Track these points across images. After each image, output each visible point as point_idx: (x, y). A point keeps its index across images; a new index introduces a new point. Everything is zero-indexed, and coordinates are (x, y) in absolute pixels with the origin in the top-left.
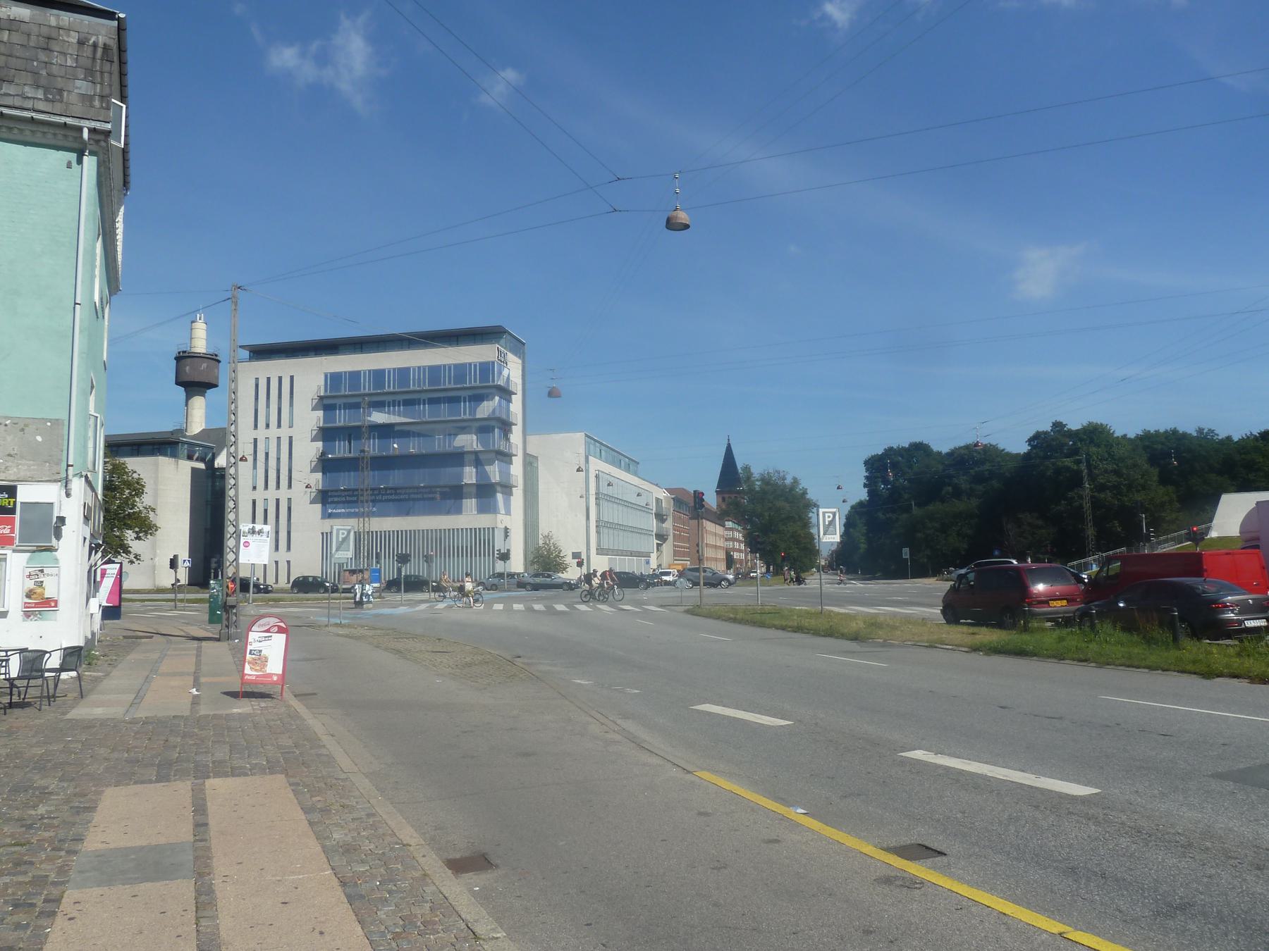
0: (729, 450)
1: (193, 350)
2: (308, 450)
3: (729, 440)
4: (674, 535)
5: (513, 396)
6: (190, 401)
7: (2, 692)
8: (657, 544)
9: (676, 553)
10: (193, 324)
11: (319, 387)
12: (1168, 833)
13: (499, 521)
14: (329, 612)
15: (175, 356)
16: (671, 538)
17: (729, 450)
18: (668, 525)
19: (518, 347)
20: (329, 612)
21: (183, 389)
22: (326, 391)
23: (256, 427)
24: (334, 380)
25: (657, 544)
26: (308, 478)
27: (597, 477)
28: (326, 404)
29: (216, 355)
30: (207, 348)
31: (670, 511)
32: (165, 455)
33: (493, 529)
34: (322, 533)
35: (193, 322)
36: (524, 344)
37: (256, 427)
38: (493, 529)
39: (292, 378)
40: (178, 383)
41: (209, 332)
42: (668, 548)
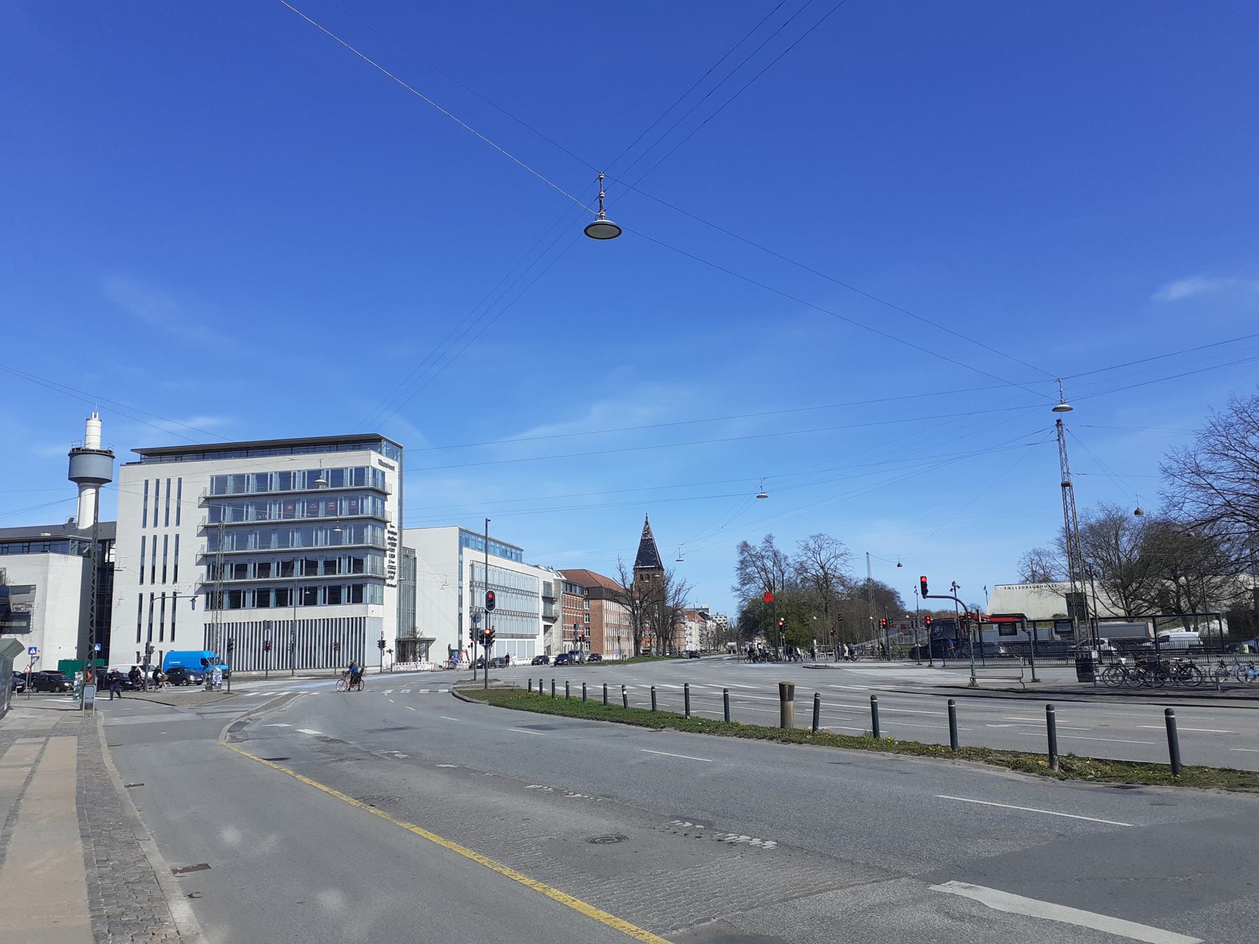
0: (647, 531)
1: (87, 447)
2: (194, 546)
3: (647, 518)
4: (564, 616)
5: (388, 496)
6: (83, 493)
7: (2, 731)
8: (545, 626)
9: (564, 635)
10: (88, 421)
11: (205, 489)
12: (105, 845)
13: (370, 611)
14: (229, 687)
15: (69, 452)
16: (560, 619)
17: (647, 531)
18: (556, 607)
19: (396, 450)
20: (229, 687)
21: (76, 484)
22: (212, 492)
23: (144, 525)
24: (220, 482)
25: (545, 626)
26: (193, 575)
27: (472, 566)
28: (213, 503)
29: (110, 452)
30: (102, 444)
31: (560, 594)
32: (56, 552)
33: (364, 618)
34: (205, 625)
35: (87, 420)
36: (401, 447)
37: (144, 525)
38: (364, 618)
39: (180, 480)
40: (70, 479)
41: (103, 428)
42: (556, 628)
